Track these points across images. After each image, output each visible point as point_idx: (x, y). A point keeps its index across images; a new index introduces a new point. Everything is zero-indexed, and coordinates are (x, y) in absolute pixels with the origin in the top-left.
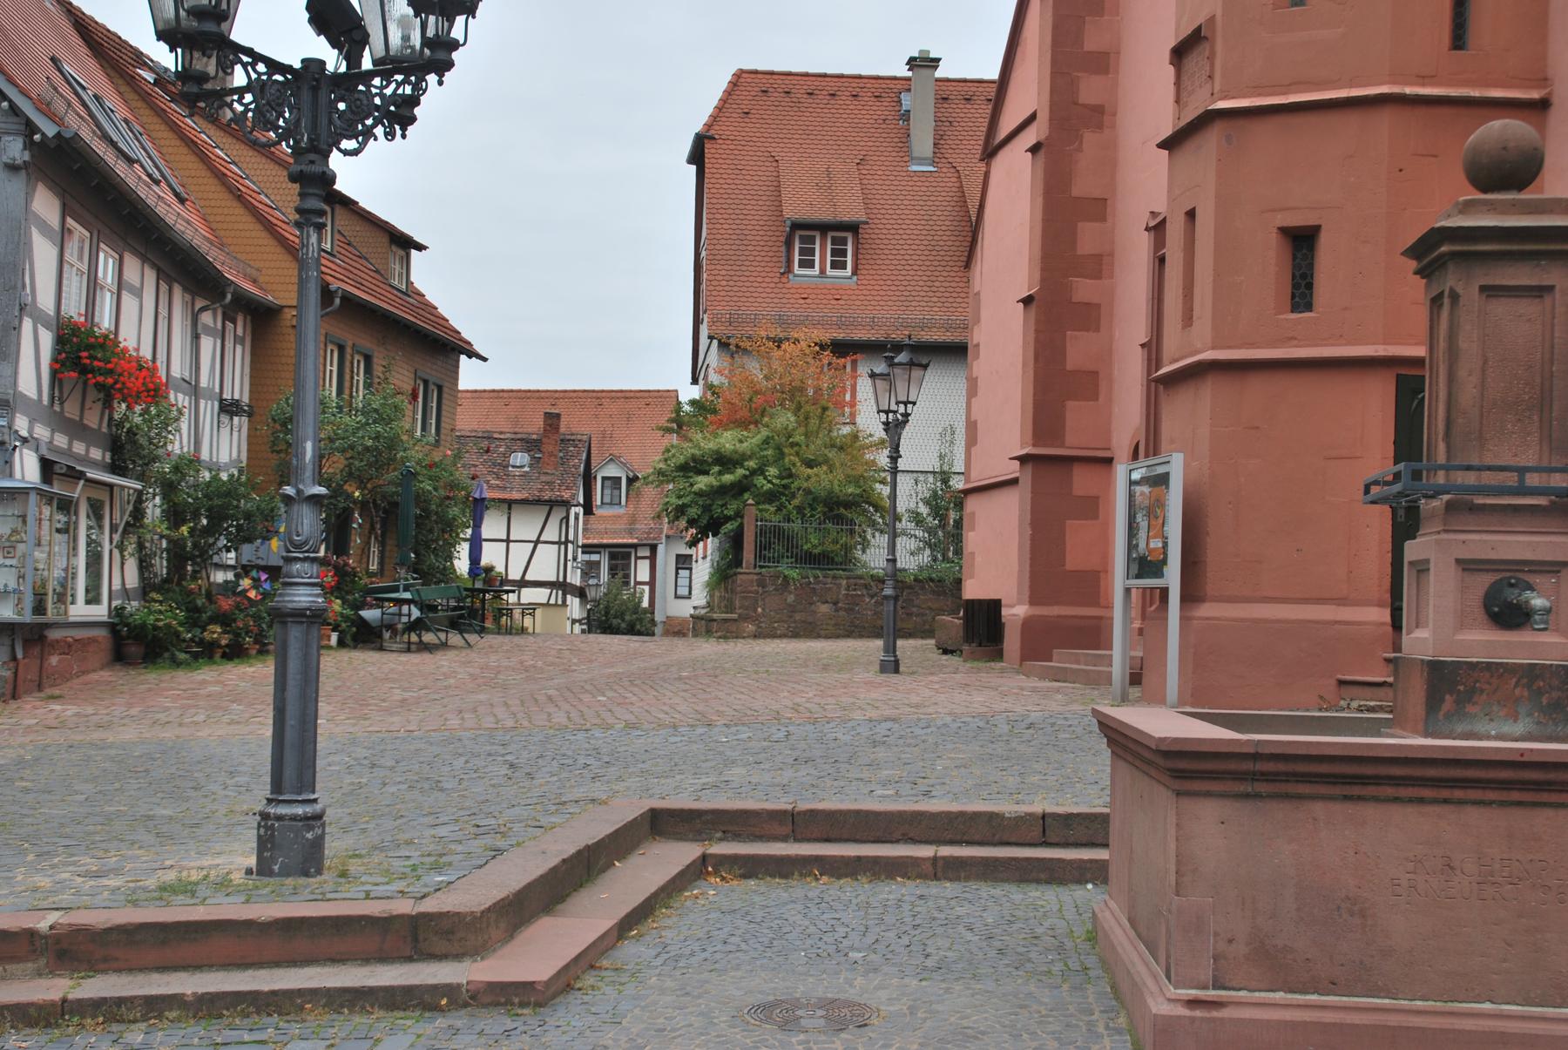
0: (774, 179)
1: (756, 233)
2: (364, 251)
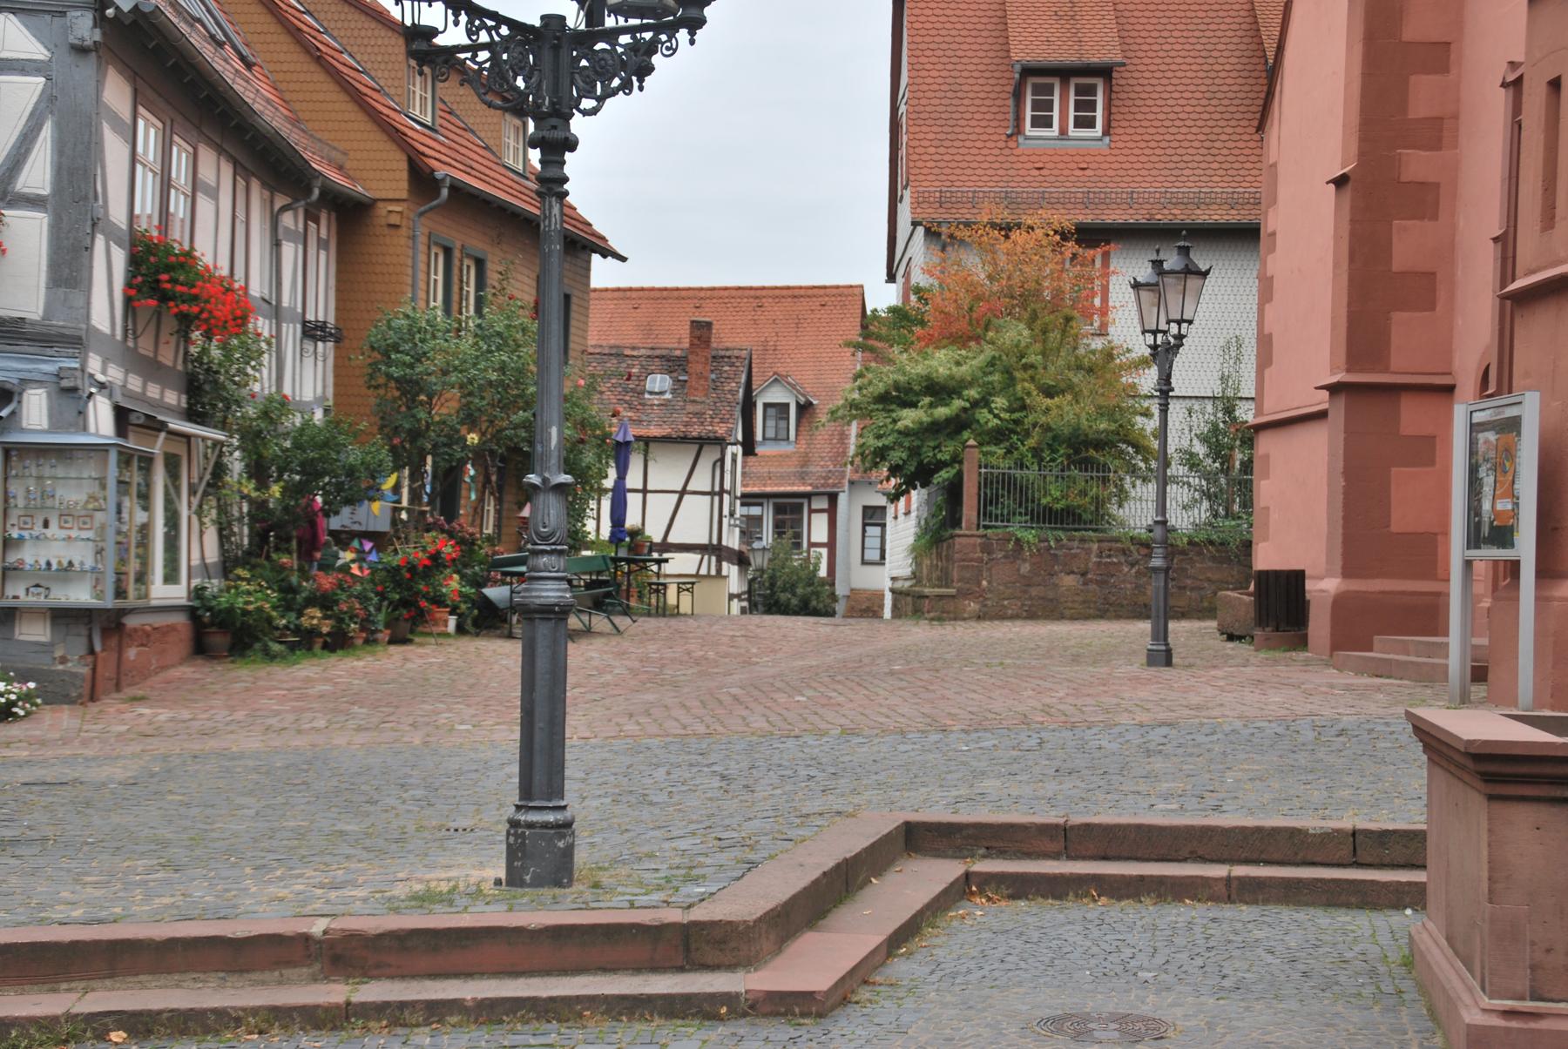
0: (998, 20)
1: (974, 81)
2: (470, 121)
